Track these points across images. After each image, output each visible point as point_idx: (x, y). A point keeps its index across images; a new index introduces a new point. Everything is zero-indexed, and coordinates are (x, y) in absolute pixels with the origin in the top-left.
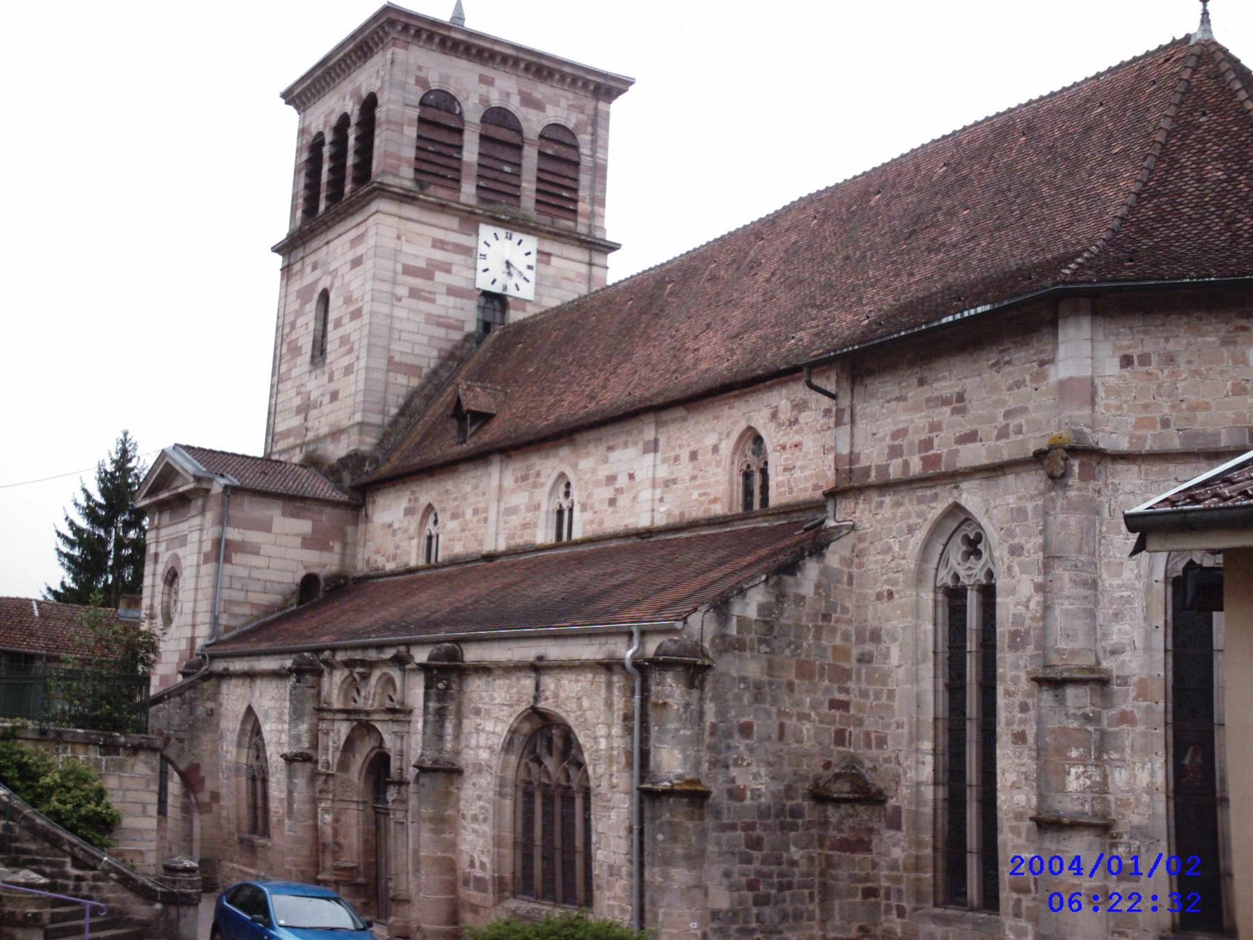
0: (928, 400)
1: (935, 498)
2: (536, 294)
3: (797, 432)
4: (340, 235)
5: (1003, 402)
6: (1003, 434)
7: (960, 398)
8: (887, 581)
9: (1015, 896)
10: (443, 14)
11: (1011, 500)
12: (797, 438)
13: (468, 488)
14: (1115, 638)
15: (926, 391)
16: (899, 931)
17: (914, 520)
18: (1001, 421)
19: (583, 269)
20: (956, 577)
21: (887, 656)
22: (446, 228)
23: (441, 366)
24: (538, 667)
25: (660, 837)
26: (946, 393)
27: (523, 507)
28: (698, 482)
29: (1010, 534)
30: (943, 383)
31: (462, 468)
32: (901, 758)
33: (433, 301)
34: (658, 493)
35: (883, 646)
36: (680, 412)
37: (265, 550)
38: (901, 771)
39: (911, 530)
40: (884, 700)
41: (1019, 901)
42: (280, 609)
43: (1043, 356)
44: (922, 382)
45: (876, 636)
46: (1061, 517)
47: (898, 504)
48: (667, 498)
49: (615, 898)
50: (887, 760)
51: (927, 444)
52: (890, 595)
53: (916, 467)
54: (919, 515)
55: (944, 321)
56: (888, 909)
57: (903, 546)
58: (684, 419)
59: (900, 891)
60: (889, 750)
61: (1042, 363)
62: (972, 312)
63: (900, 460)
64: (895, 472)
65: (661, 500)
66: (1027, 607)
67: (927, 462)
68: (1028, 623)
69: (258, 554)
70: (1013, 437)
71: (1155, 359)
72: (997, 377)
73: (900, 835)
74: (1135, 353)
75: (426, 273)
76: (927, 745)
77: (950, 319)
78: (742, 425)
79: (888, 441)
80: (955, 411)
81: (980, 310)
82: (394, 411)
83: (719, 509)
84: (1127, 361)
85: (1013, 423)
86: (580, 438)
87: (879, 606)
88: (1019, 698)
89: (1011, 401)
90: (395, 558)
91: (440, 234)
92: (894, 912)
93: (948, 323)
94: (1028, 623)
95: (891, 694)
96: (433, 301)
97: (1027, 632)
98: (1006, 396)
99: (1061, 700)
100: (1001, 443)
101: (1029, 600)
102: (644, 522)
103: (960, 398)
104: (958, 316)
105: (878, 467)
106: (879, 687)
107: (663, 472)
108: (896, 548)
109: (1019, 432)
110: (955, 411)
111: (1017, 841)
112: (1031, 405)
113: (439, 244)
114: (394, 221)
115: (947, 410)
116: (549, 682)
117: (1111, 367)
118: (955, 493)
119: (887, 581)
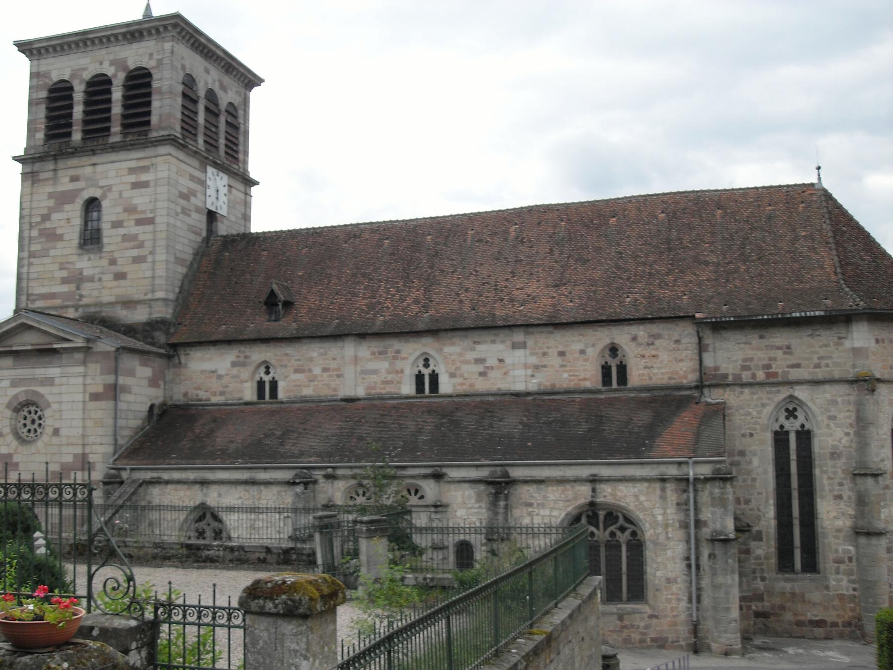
0: (766, 346)
1: (779, 392)
2: (228, 213)
3: (653, 349)
4: (113, 162)
5: (817, 353)
6: (818, 366)
7: (788, 347)
8: (749, 429)
9: (836, 565)
10: (135, 14)
11: (828, 396)
12: (654, 353)
13: (315, 354)
14: (882, 455)
15: (765, 342)
16: (762, 588)
17: (765, 401)
18: (816, 361)
19: (242, 196)
20: (782, 427)
21: (750, 462)
22: (190, 166)
23: (194, 259)
24: (594, 480)
25: (730, 561)
26: (778, 344)
27: (383, 370)
28: (568, 368)
29: (828, 410)
30: (776, 340)
31: (304, 341)
32: (761, 508)
33: (189, 216)
34: (529, 372)
35: (747, 458)
36: (550, 329)
37: (135, 389)
38: (761, 514)
39: (763, 405)
40: (749, 482)
41: (838, 568)
42: (142, 429)
43: (840, 335)
44: (761, 337)
45: (742, 453)
46: (872, 407)
47: (753, 393)
48: (537, 375)
49: (672, 594)
50: (750, 510)
51: (769, 366)
52: (751, 435)
53: (761, 376)
54: (769, 399)
55: (794, 315)
56: (755, 578)
57: (759, 413)
58: (552, 333)
59: (762, 570)
60: (753, 505)
61: (840, 338)
62: (812, 313)
63: (749, 373)
64: (746, 376)
65: (532, 376)
66: (840, 442)
67: (768, 375)
68: (841, 449)
69: (130, 392)
70: (824, 368)
71: (886, 341)
72: (812, 341)
73: (762, 543)
74: (879, 338)
75: (185, 197)
76: (771, 502)
77: (798, 315)
78: (607, 341)
79: (740, 362)
80: (785, 353)
81: (817, 313)
82: (177, 290)
83: (588, 385)
84: (877, 341)
85: (823, 362)
86: (442, 334)
87: (743, 440)
88: (837, 481)
89: (822, 352)
90: (222, 393)
91: (133, 164)
92: (759, 579)
93: (797, 318)
94: (841, 449)
95: (754, 480)
96: (189, 216)
97: (841, 453)
98: (818, 349)
99: (877, 482)
100: (817, 370)
101: (841, 439)
102: (520, 387)
103: (788, 347)
104: (803, 314)
105: (734, 375)
106: (745, 477)
107: (533, 360)
108: (754, 413)
109: (827, 366)
110: (785, 353)
111: (837, 541)
112: (834, 356)
113: (132, 171)
114: (174, 161)
115: (780, 352)
116: (601, 487)
117: (873, 343)
118: (791, 390)
119: (749, 429)
